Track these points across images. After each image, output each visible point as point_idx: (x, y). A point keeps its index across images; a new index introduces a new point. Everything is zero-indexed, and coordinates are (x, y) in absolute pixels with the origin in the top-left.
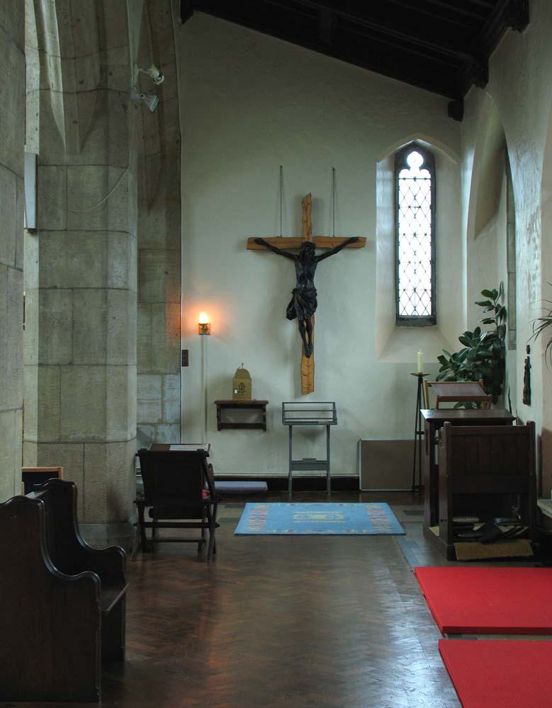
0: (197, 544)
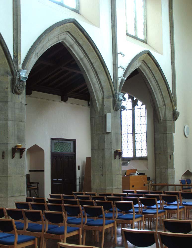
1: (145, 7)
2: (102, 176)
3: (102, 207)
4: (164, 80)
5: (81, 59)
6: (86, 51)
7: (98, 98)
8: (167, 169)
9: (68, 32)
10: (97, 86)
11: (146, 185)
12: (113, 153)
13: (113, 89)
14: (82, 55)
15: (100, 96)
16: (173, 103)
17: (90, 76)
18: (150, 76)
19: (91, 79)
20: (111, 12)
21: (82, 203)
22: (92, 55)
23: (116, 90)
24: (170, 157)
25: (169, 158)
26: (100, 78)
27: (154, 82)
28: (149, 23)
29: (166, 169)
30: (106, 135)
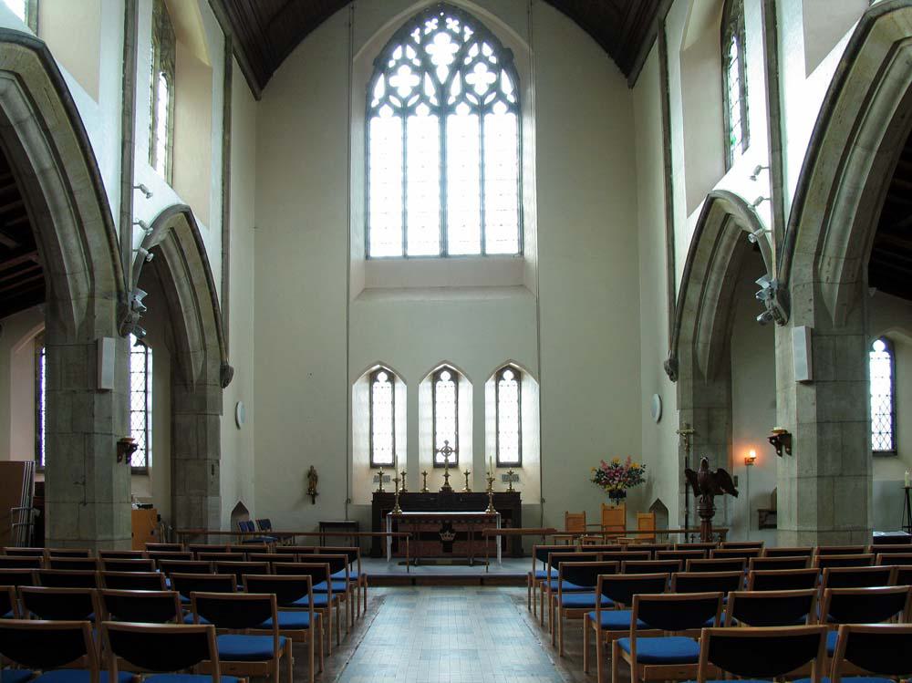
0: (318, 537)
1: (172, 110)
2: (81, 506)
3: (178, 592)
4: (210, 288)
5: (43, 172)
6: (60, 152)
7: (78, 294)
8: (204, 498)
9: (18, 76)
10: (78, 260)
11: (156, 532)
12: (114, 444)
13: (121, 276)
14: (47, 162)
15: (84, 289)
16: (223, 346)
17: (61, 228)
18: (181, 273)
19: (64, 237)
20: (122, 75)
21: (841, 609)
22: (75, 168)
23: (126, 283)
24: (213, 470)
25: (209, 472)
26: (89, 239)
27: (186, 289)
28: (179, 148)
29: (204, 496)
30: (96, 397)
